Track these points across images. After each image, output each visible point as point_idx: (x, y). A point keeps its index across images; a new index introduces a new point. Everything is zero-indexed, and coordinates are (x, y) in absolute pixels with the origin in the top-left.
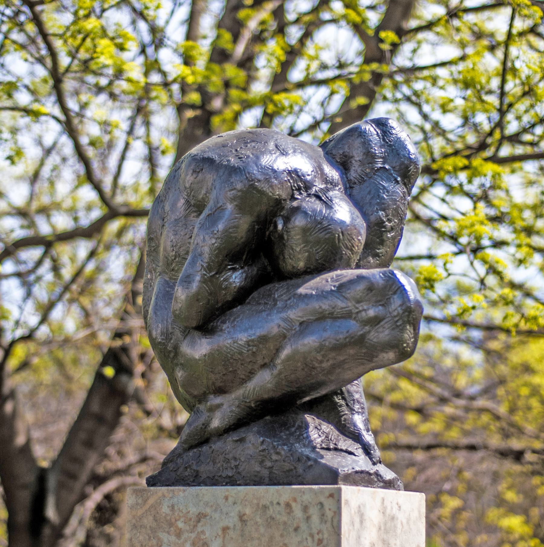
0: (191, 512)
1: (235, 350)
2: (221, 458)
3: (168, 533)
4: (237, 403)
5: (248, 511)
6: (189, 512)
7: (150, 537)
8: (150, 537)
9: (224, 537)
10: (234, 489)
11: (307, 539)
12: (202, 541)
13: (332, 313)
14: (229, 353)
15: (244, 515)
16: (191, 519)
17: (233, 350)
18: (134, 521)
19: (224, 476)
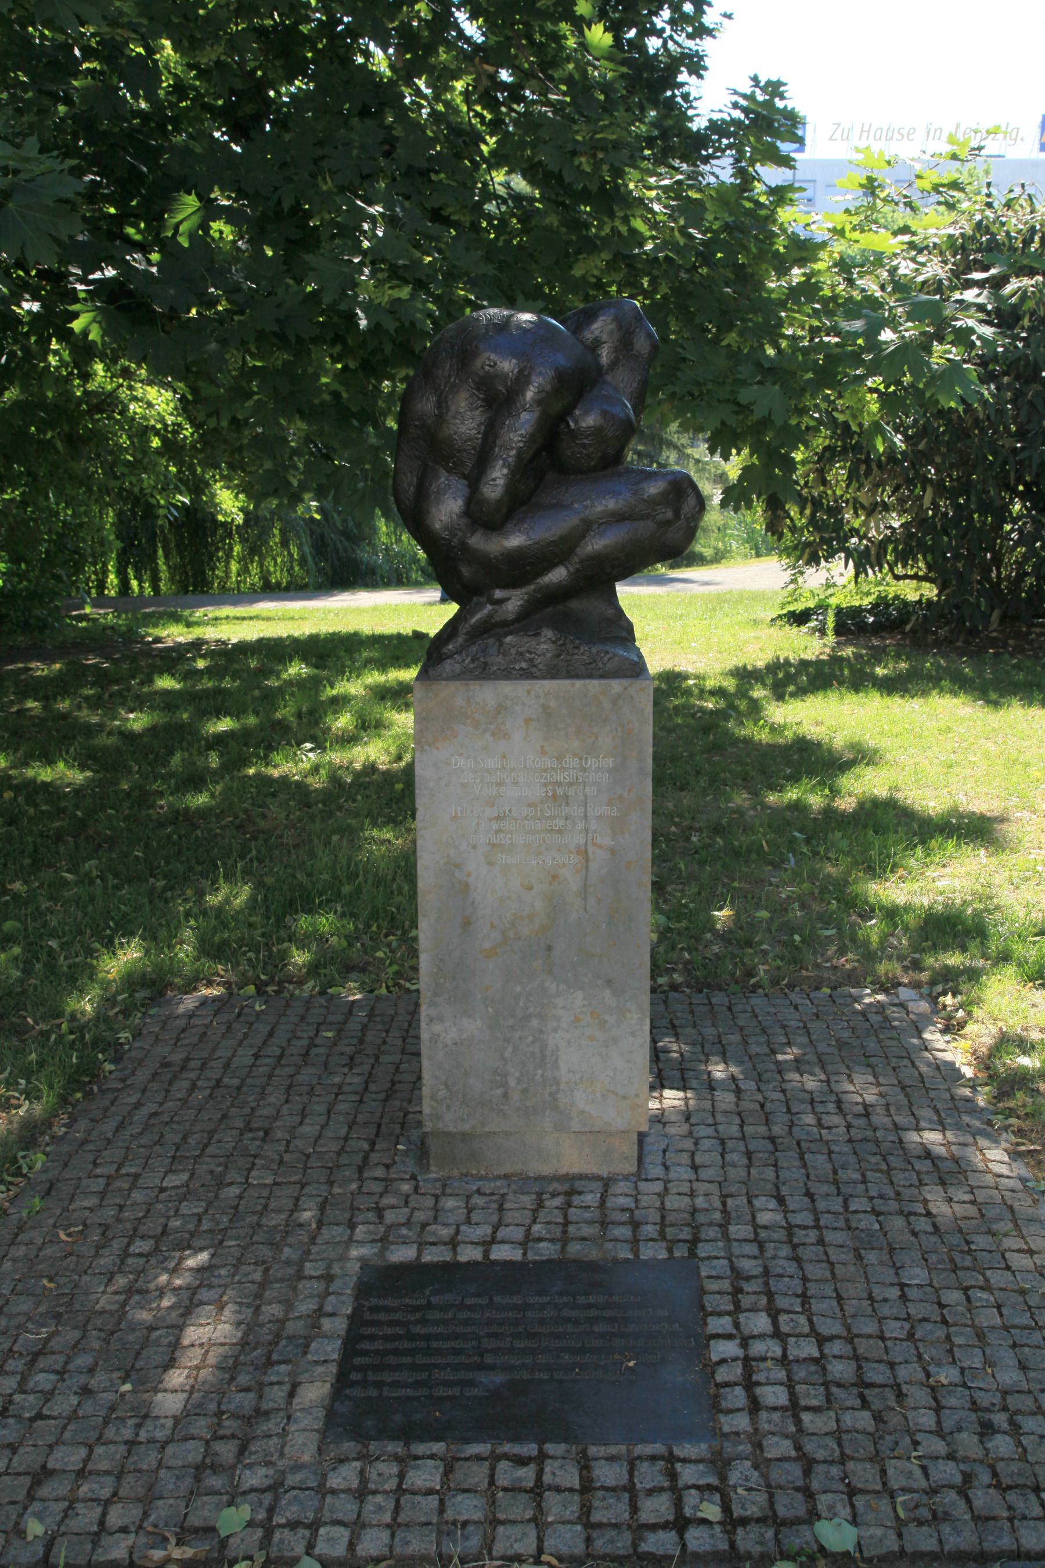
2: (513, 651)
5: (552, 704)
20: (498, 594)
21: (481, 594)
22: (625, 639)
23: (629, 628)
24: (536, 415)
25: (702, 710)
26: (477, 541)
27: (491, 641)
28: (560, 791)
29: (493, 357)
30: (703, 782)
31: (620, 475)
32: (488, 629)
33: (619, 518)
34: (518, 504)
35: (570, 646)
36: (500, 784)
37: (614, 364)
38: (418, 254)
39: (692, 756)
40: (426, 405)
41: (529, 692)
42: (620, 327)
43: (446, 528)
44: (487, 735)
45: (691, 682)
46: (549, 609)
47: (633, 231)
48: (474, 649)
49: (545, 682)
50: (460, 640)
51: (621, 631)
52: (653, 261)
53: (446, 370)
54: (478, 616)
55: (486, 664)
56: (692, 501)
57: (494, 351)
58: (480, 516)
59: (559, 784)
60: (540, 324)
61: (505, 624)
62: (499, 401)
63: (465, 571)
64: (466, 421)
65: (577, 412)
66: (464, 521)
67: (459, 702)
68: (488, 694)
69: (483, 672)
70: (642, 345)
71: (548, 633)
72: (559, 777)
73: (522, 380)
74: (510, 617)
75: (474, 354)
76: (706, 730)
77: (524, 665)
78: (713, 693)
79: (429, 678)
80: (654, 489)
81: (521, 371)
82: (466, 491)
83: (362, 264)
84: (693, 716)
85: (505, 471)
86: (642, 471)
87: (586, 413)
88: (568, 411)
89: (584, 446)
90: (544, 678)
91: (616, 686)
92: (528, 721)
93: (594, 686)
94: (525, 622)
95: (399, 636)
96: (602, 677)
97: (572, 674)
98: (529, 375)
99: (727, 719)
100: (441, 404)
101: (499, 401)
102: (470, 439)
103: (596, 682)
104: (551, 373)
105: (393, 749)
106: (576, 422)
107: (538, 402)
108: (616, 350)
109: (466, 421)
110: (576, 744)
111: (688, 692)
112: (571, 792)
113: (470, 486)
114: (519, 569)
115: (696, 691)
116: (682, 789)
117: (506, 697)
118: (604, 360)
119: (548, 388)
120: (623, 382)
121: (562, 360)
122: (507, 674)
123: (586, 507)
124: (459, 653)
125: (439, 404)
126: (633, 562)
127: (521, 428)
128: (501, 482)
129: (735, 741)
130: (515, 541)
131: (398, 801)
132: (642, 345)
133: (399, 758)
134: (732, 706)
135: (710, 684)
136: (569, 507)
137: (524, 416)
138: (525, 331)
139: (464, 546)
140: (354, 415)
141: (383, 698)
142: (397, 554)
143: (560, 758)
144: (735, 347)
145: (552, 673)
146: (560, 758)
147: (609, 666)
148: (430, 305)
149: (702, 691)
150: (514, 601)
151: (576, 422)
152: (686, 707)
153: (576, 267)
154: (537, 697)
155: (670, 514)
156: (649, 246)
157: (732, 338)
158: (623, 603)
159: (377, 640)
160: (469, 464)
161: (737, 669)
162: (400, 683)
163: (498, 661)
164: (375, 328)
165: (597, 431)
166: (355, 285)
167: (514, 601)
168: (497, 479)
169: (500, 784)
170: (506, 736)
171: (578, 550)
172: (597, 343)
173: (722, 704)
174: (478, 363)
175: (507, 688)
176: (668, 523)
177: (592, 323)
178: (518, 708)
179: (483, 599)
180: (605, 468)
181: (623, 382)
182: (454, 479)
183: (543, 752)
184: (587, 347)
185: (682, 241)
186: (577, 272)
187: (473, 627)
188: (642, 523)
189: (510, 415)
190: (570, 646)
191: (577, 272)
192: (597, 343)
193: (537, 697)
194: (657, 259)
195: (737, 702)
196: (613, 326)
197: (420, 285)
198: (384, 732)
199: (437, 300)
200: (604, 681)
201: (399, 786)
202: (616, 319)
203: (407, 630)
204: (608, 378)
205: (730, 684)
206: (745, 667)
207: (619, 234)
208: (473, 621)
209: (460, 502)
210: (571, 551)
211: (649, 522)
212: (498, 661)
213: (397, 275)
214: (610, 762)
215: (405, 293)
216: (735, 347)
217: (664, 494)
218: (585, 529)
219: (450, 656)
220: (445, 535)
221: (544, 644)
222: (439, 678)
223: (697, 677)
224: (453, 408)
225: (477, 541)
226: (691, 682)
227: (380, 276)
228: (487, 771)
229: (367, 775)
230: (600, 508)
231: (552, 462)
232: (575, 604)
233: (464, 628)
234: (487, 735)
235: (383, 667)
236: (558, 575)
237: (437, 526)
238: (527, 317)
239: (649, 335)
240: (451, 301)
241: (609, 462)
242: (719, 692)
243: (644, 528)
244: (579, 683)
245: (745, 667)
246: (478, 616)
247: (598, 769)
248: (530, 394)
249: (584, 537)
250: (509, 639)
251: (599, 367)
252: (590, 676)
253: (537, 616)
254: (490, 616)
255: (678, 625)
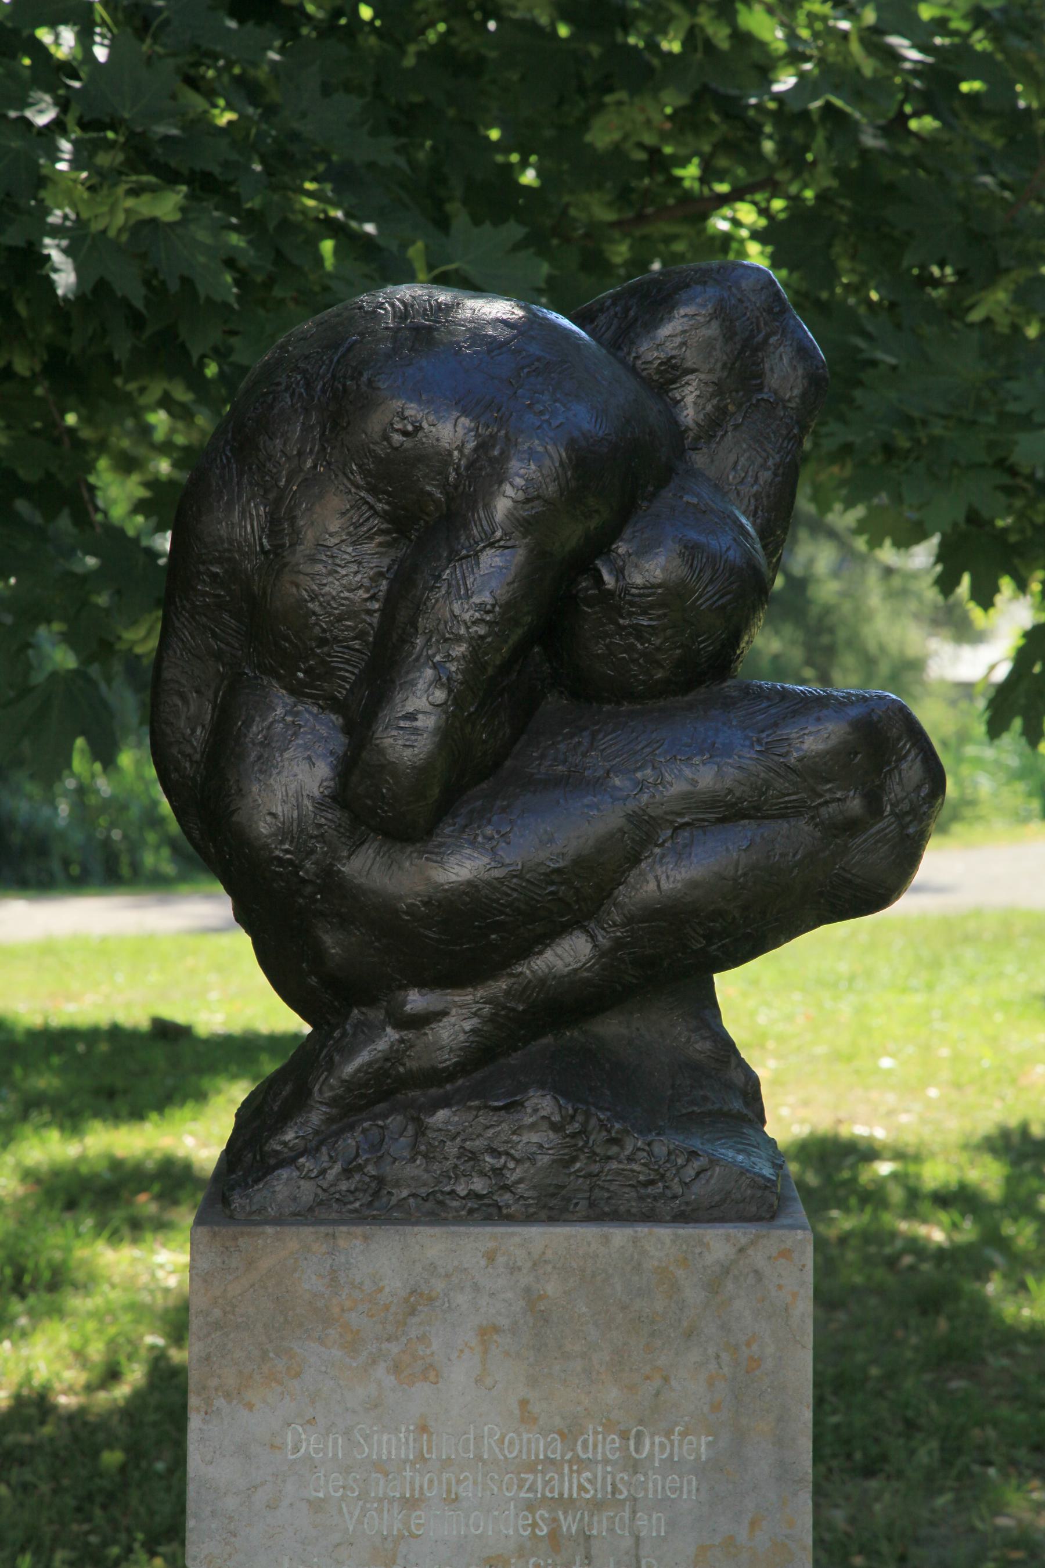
0: (387, 1290)
1: (515, 895)
2: (452, 1149)
3: (321, 1341)
4: (487, 1009)
5: (552, 1288)
6: (381, 1290)
7: (264, 1354)
8: (264, 1354)
9: (486, 1352)
10: (513, 1234)
11: (718, 1357)
12: (420, 1362)
13: (757, 809)
14: (497, 901)
15: (541, 1297)
16: (387, 1307)
17: (509, 895)
18: (217, 1313)
19: (463, 1194)
20: (416, 1001)
21: (372, 1002)
22: (741, 1118)
23: (752, 1085)
24: (520, 555)
25: (916, 1247)
26: (367, 868)
27: (394, 1121)
28: (569, 1524)
29: (412, 410)
30: (927, 1452)
31: (728, 704)
32: (388, 1089)
33: (726, 811)
34: (470, 777)
35: (598, 1137)
36: (411, 1503)
37: (714, 425)
38: (199, 102)
39: (891, 1376)
40: (240, 523)
41: (491, 1257)
42: (729, 335)
43: (284, 833)
44: (380, 1371)
45: (884, 1168)
46: (544, 1041)
47: (743, 39)
48: (350, 1142)
49: (534, 1232)
50: (315, 1118)
51: (730, 1093)
52: (789, 115)
53: (292, 440)
54: (363, 1057)
55: (380, 1180)
56: (912, 770)
57: (416, 395)
58: (372, 804)
59: (566, 1503)
60: (530, 329)
61: (434, 1077)
62: (423, 519)
63: (333, 943)
64: (339, 564)
65: (622, 548)
66: (335, 815)
67: (310, 1281)
68: (384, 1259)
69: (374, 1204)
70: (783, 375)
71: (543, 1104)
72: (568, 1485)
73: (485, 468)
74: (446, 1059)
75: (367, 403)
76: (932, 1301)
77: (479, 1185)
78: (943, 1199)
79: (231, 1219)
80: (814, 739)
81: (483, 446)
82: (340, 742)
83: (58, 126)
84: (891, 1262)
85: (440, 695)
86: (785, 695)
87: (645, 550)
88: (600, 545)
89: (638, 632)
90: (529, 1219)
91: (718, 1242)
92: (487, 1332)
93: (660, 1241)
94: (486, 1069)
95: (115, 1033)
96: (682, 1217)
97: (602, 1212)
98: (504, 458)
99: (982, 1272)
100: (280, 526)
101: (423, 519)
102: (352, 614)
103: (664, 1232)
104: (558, 453)
105: (96, 1351)
106: (619, 573)
107: (523, 524)
108: (719, 389)
109: (339, 564)
110: (613, 1394)
111: (873, 1197)
112: (599, 1527)
113: (348, 729)
114: (470, 938)
115: (896, 1194)
116: (869, 1471)
117: (432, 1268)
118: (689, 414)
119: (551, 490)
120: (734, 467)
121: (583, 418)
122: (436, 1208)
123: (641, 786)
124: (310, 1151)
125: (274, 525)
126: (756, 925)
127: (483, 583)
128: (427, 722)
129: (1009, 1338)
130: (461, 868)
131: (111, 1498)
132: (783, 375)
133: (112, 1375)
134: (994, 1239)
135: (935, 1174)
136: (597, 785)
137: (491, 560)
138: (494, 346)
139: (330, 880)
140: (25, 490)
141: (71, 1205)
142: (107, 805)
143: (570, 1434)
144: (1003, 325)
145: (552, 1206)
146: (570, 1434)
147: (698, 1189)
148: (235, 239)
149: (914, 1195)
150: (455, 1019)
151: (619, 573)
152: (872, 1237)
153: (598, 122)
154: (514, 1269)
155: (855, 805)
156: (785, 82)
157: (995, 302)
158: (733, 1025)
159: (55, 1042)
160: (350, 674)
161: (1005, 1134)
162: (116, 1164)
163: (411, 1174)
164: (95, 293)
165: (671, 596)
166: (42, 181)
167: (455, 1019)
168: (419, 713)
169: (411, 1503)
170: (430, 1372)
171: (622, 894)
172: (672, 372)
173: (969, 1232)
174: (376, 423)
175: (433, 1245)
176: (851, 826)
177: (655, 323)
178: (461, 1299)
179: (376, 1015)
180: (689, 686)
181: (734, 467)
182: (308, 711)
183: (526, 1415)
184: (646, 382)
185: (868, 67)
186: (602, 136)
187: (349, 1085)
188: (783, 826)
189: (454, 557)
190: (598, 1137)
191: (602, 136)
192: (672, 372)
193: (514, 1269)
194: (805, 114)
195: (1008, 1229)
196: (713, 330)
197: (205, 186)
198: (76, 1302)
199: (252, 223)
200: (686, 1231)
201: (112, 1458)
202: (722, 313)
203: (134, 1013)
204: (699, 459)
205: (988, 1176)
206: (1024, 1130)
207: (709, 46)
208: (350, 1069)
209: (323, 770)
210: (604, 893)
211: (803, 825)
212: (411, 1174)
213: (148, 160)
214: (702, 1446)
215: (167, 206)
216: (1003, 325)
217: (842, 754)
218: (642, 837)
219: (290, 1161)
220: (283, 850)
221: (532, 1131)
222: (258, 1218)
223: (899, 1155)
224: (310, 536)
225: (367, 868)
226: (884, 1168)
227: (103, 159)
228: (379, 1466)
229: (27, 1425)
230: (678, 787)
231: (563, 669)
232: (611, 1027)
233: (325, 1089)
234: (380, 1371)
235: (70, 1117)
236: (570, 954)
237: (264, 828)
238: (498, 309)
239: (803, 352)
240: (286, 226)
241: (702, 668)
242: (958, 1199)
243: (790, 838)
244: (620, 1235)
245: (1024, 1130)
246: (363, 1057)
247: (671, 1465)
248: (502, 506)
249: (635, 860)
250: (442, 1115)
251: (677, 432)
252: (650, 1217)
253: (515, 1059)
254: (394, 1056)
255: (845, 1009)
